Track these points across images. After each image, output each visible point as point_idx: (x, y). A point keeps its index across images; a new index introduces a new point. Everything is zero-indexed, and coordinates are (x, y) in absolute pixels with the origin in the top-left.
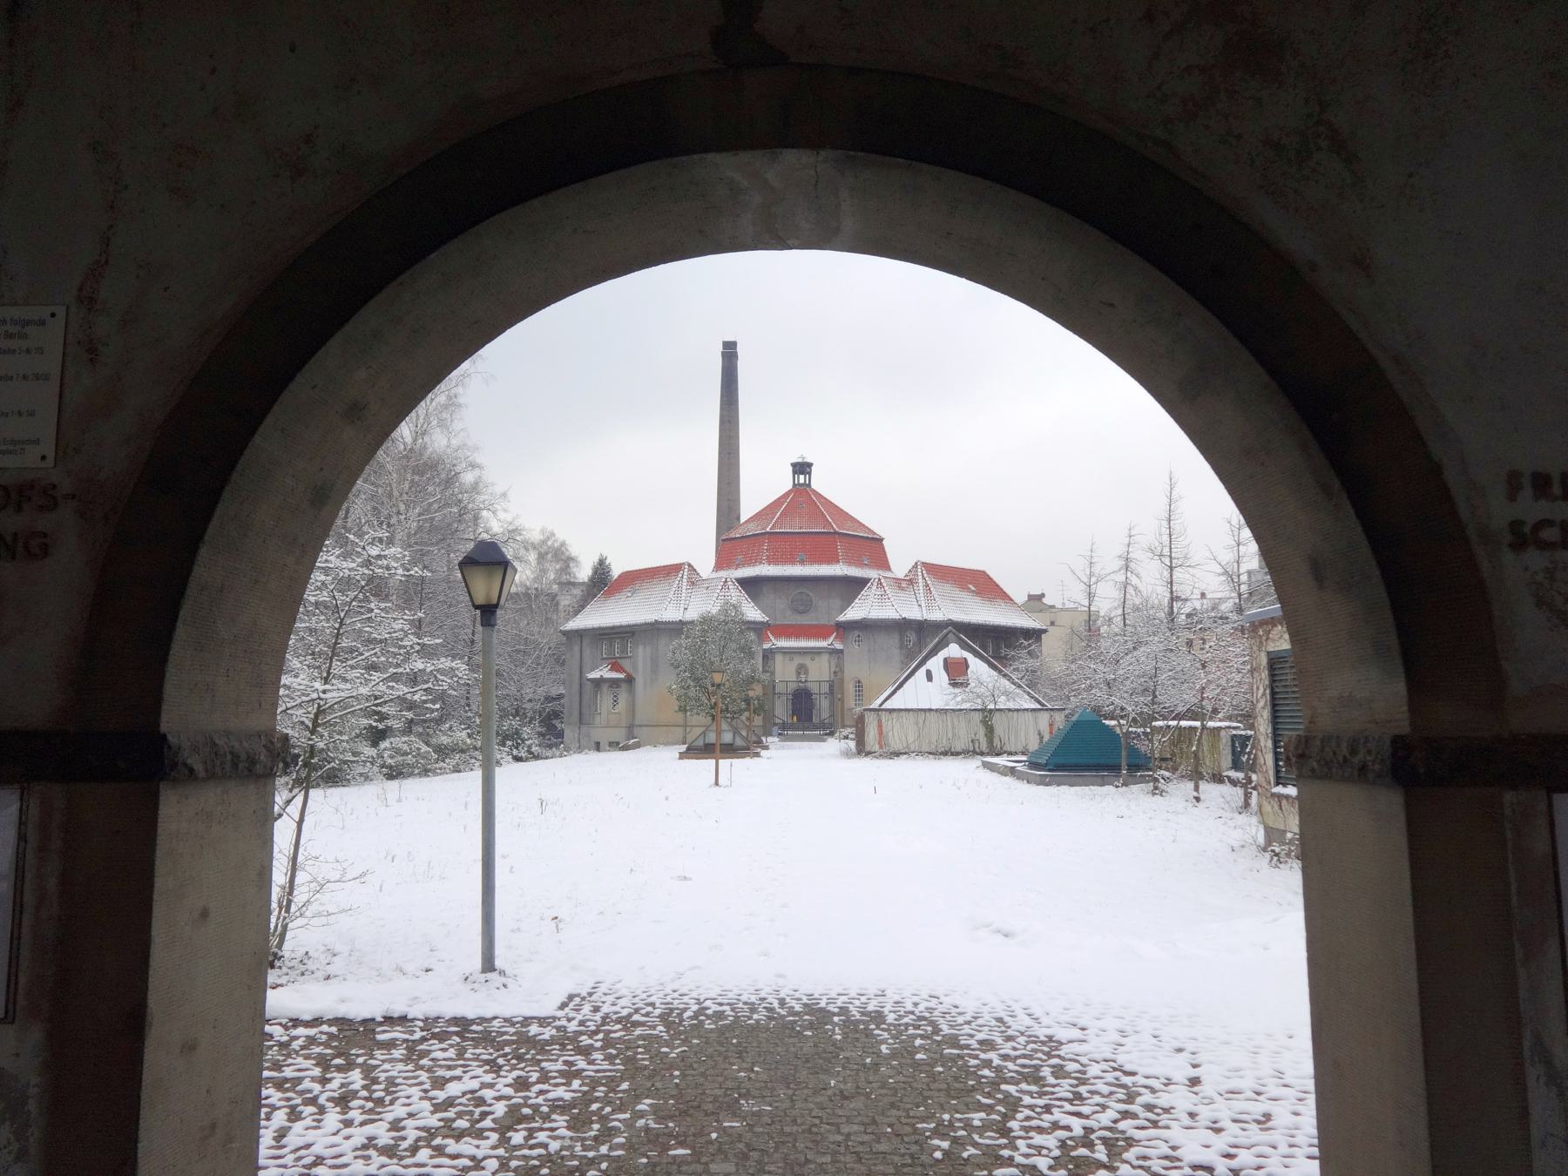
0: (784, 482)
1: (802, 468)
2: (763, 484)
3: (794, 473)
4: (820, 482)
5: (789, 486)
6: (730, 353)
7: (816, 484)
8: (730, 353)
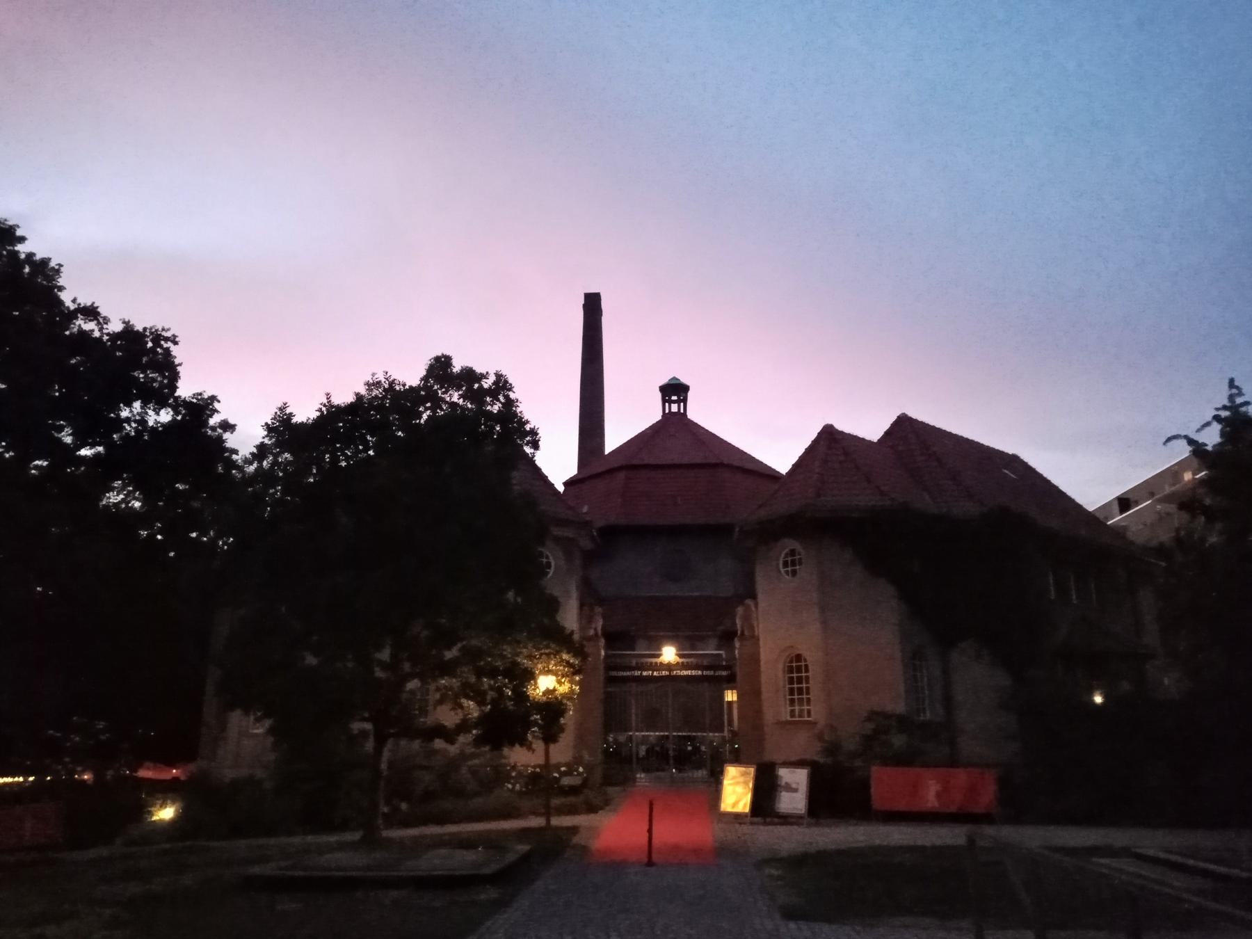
0: (650, 413)
1: (674, 391)
3: (666, 400)
4: (698, 412)
5: (656, 416)
6: (592, 305)
7: (693, 415)
8: (592, 305)
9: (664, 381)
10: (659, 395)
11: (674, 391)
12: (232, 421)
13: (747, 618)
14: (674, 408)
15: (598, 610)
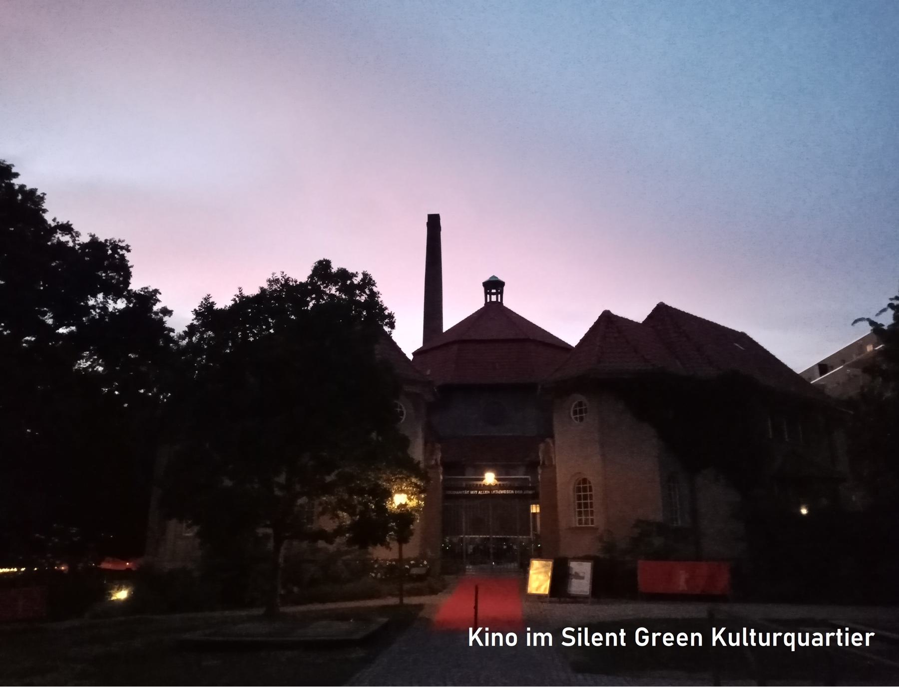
1: (494, 286)
2: (460, 305)
5: (481, 304)
6: (434, 223)
7: (506, 303)
8: (434, 223)
9: (486, 278)
10: (483, 289)
11: (494, 286)
12: (169, 308)
13: (547, 452)
14: (494, 298)
15: (438, 446)
